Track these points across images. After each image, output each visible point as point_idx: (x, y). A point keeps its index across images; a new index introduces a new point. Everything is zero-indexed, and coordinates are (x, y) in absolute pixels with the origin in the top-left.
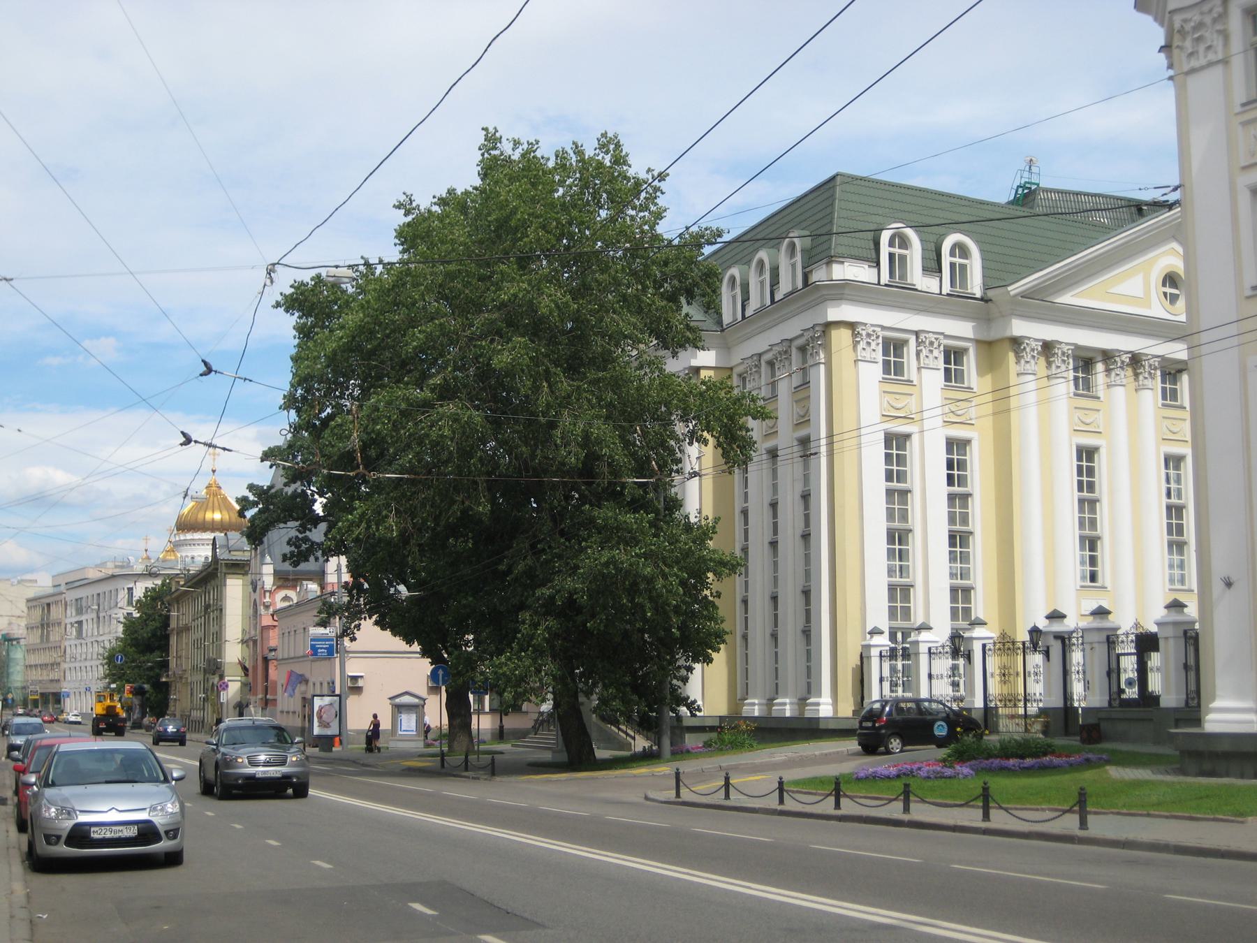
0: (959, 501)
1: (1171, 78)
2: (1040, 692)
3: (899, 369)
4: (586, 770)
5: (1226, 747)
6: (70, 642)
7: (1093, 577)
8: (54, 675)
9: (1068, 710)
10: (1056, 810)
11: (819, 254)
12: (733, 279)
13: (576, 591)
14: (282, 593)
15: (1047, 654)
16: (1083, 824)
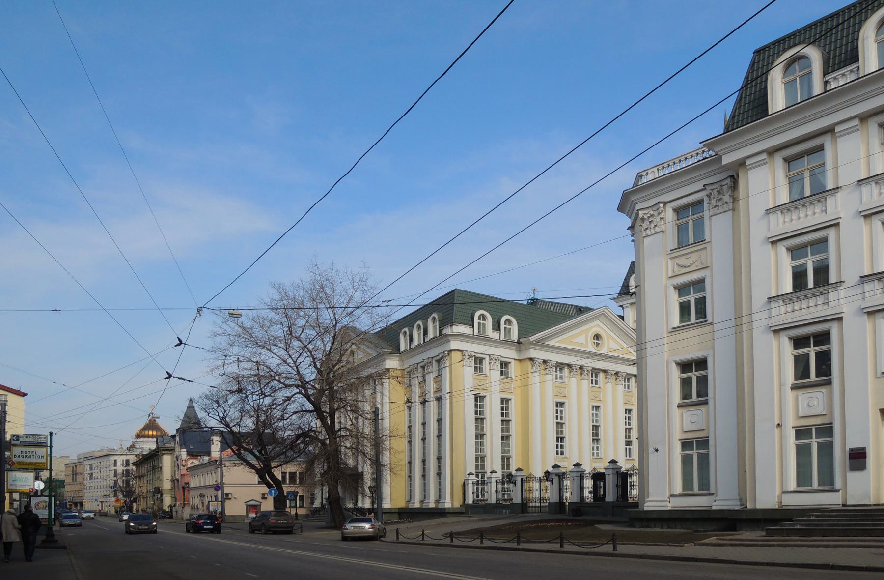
0: (505, 422)
1: (633, 241)
2: (550, 494)
3: (481, 370)
5: (655, 516)
6: (88, 482)
8: (80, 495)
9: (561, 504)
11: (446, 322)
12: (405, 333)
13: (29, 495)
14: (191, 461)
15: (552, 482)
16: (615, 548)
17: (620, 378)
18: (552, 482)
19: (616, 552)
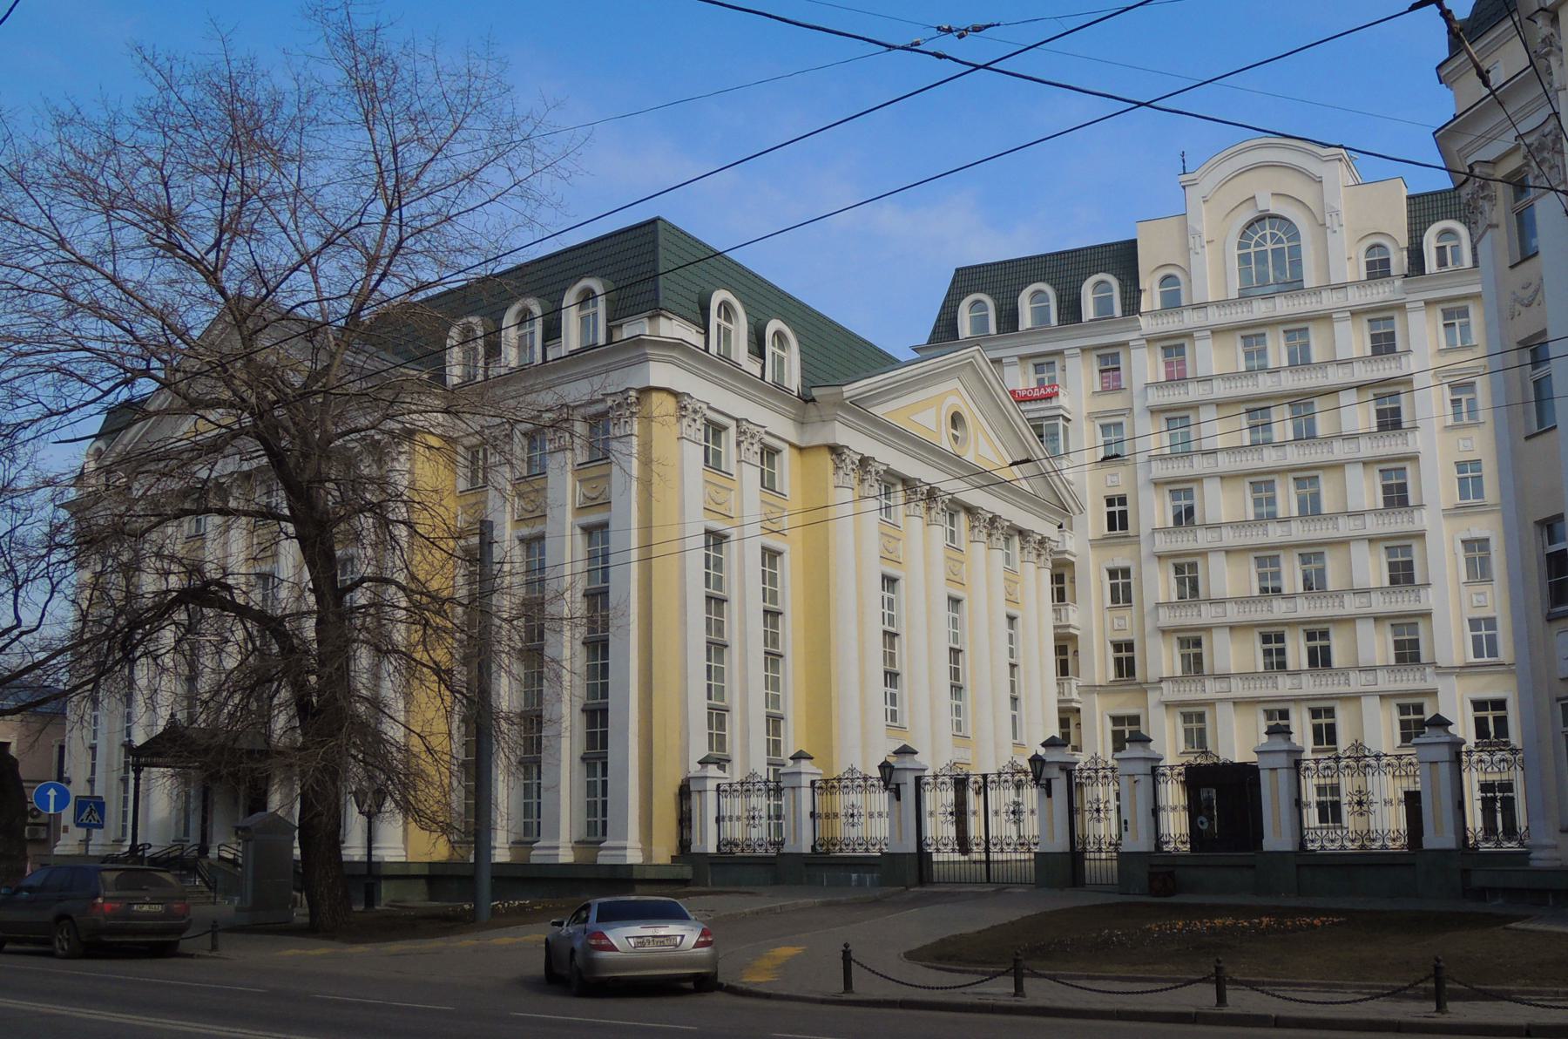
4: (403, 937)
7: (894, 718)
10: (983, 973)
15: (1048, 790)
17: (997, 534)
18: (1048, 790)
19: (1226, 1010)
